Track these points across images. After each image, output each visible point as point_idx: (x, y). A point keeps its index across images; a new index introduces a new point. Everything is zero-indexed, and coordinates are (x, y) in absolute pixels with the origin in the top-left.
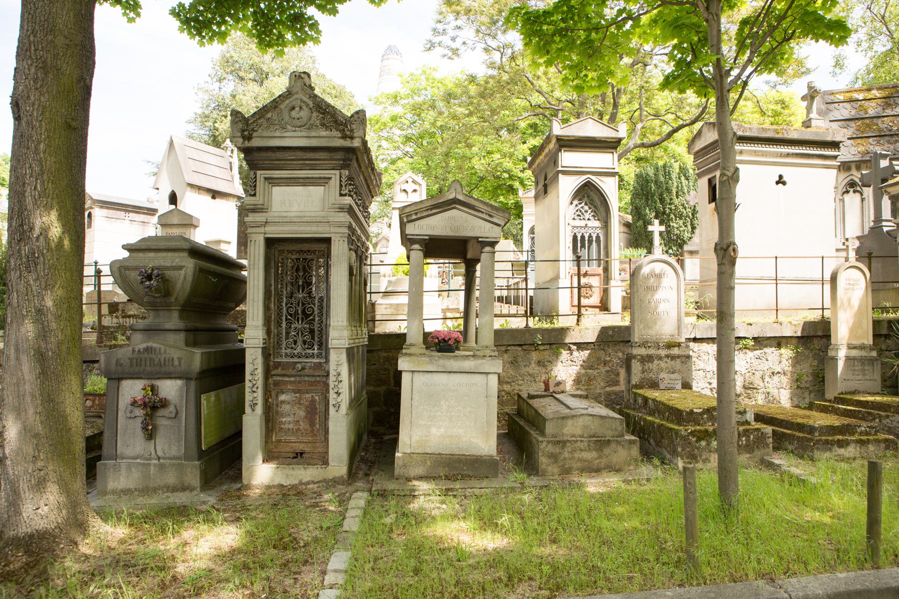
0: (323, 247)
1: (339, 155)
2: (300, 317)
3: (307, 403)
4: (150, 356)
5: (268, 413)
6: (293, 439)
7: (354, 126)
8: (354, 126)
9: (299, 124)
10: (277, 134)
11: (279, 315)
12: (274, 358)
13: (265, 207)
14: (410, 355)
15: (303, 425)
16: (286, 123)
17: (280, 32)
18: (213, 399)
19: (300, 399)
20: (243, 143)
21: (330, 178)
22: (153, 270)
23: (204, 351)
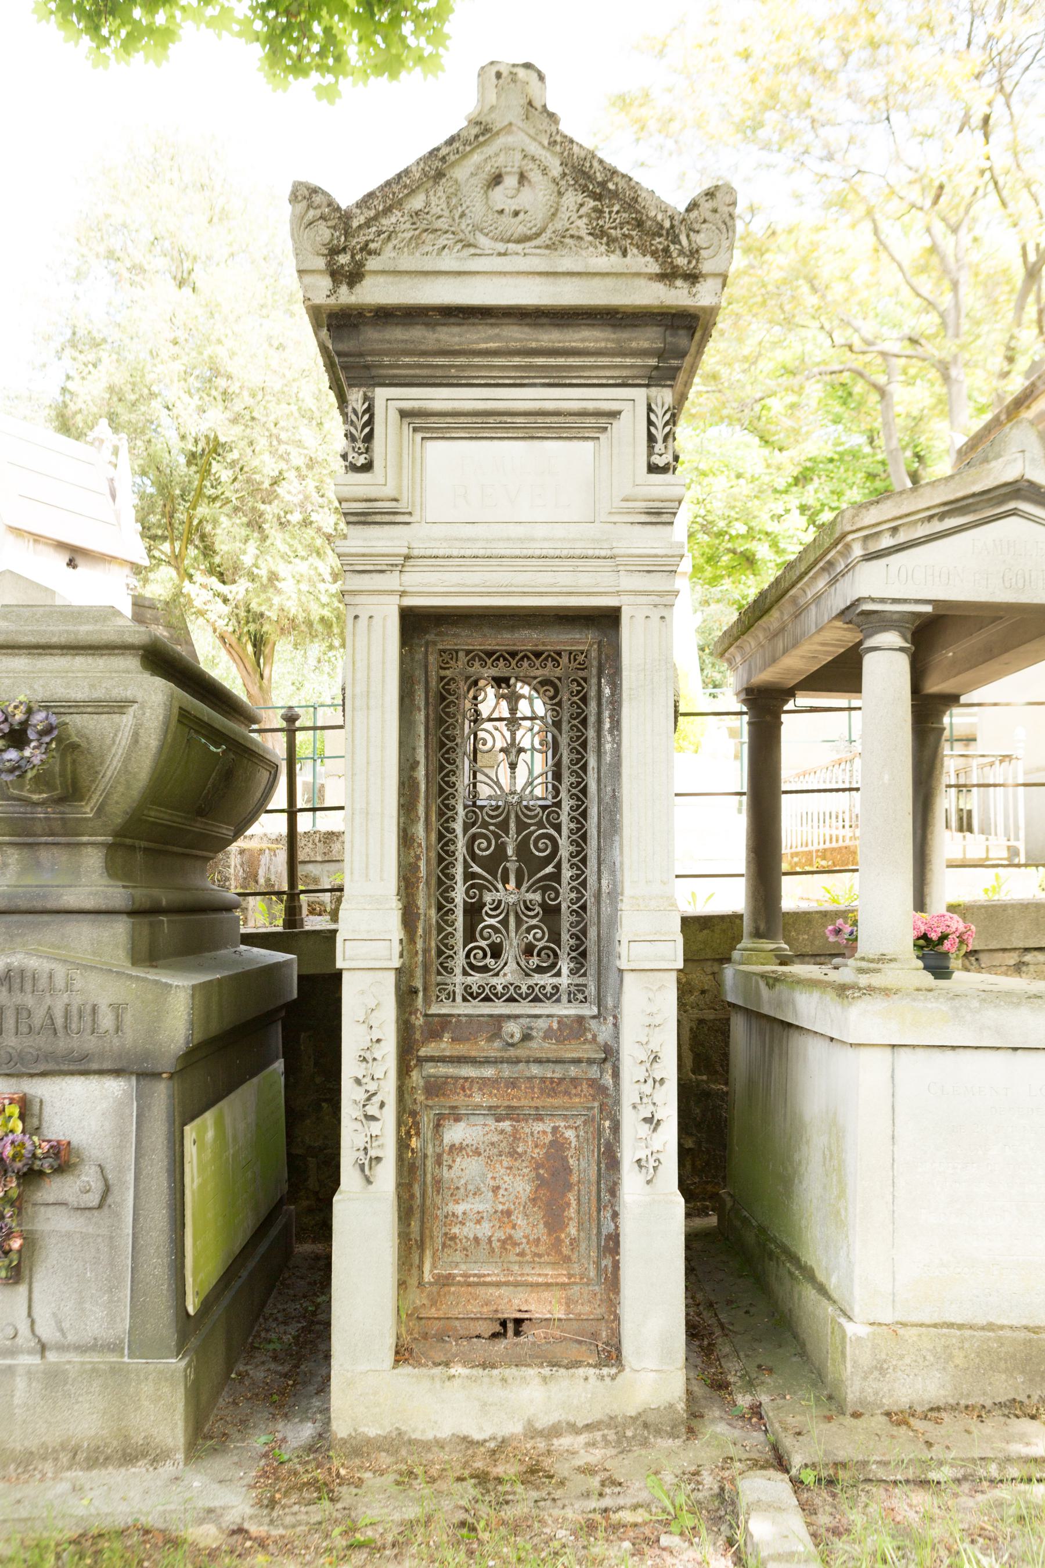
0: (583, 640)
1: (647, 338)
2: (512, 866)
3: (538, 1154)
4: (18, 998)
5: (410, 1185)
6: (492, 1272)
7: (700, 239)
8: (700, 239)
9: (521, 230)
10: (448, 262)
11: (444, 859)
12: (427, 1002)
13: (402, 506)
14: (886, 992)
15: (527, 1227)
16: (477, 228)
17: (328, 31)
18: (210, 1134)
19: (515, 1136)
20: (333, 292)
21: (615, 414)
22: (29, 711)
23: (194, 982)
